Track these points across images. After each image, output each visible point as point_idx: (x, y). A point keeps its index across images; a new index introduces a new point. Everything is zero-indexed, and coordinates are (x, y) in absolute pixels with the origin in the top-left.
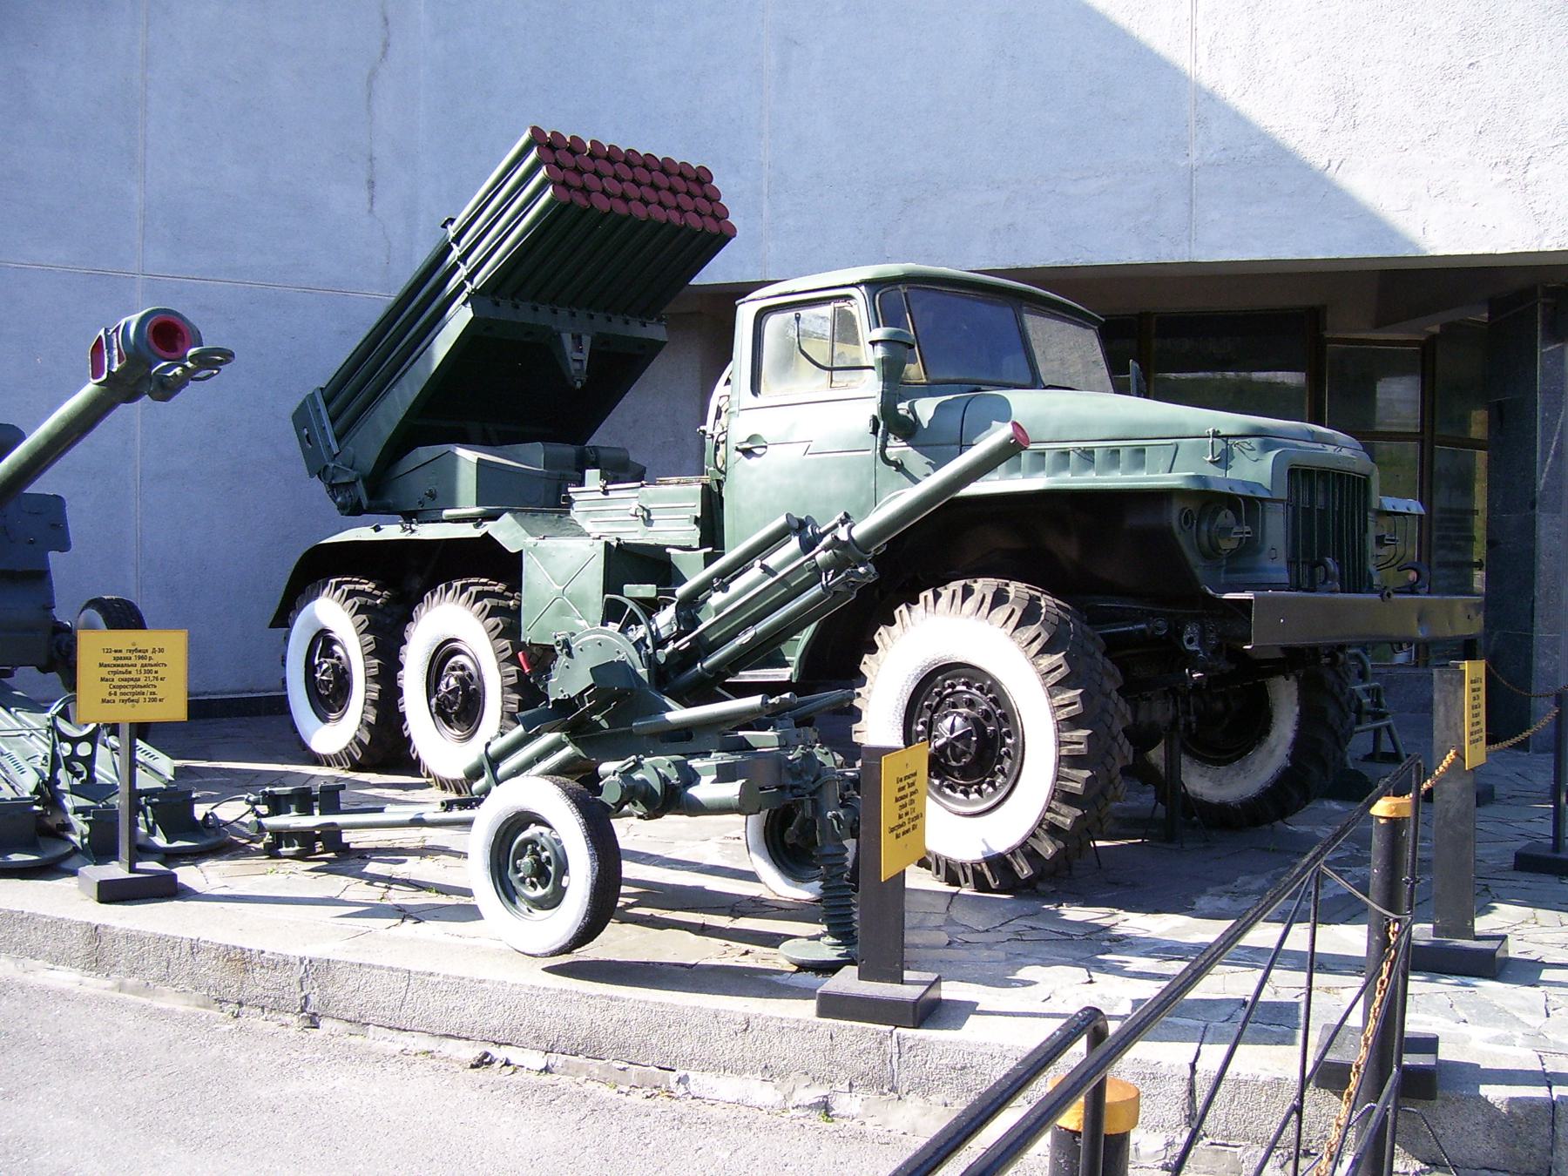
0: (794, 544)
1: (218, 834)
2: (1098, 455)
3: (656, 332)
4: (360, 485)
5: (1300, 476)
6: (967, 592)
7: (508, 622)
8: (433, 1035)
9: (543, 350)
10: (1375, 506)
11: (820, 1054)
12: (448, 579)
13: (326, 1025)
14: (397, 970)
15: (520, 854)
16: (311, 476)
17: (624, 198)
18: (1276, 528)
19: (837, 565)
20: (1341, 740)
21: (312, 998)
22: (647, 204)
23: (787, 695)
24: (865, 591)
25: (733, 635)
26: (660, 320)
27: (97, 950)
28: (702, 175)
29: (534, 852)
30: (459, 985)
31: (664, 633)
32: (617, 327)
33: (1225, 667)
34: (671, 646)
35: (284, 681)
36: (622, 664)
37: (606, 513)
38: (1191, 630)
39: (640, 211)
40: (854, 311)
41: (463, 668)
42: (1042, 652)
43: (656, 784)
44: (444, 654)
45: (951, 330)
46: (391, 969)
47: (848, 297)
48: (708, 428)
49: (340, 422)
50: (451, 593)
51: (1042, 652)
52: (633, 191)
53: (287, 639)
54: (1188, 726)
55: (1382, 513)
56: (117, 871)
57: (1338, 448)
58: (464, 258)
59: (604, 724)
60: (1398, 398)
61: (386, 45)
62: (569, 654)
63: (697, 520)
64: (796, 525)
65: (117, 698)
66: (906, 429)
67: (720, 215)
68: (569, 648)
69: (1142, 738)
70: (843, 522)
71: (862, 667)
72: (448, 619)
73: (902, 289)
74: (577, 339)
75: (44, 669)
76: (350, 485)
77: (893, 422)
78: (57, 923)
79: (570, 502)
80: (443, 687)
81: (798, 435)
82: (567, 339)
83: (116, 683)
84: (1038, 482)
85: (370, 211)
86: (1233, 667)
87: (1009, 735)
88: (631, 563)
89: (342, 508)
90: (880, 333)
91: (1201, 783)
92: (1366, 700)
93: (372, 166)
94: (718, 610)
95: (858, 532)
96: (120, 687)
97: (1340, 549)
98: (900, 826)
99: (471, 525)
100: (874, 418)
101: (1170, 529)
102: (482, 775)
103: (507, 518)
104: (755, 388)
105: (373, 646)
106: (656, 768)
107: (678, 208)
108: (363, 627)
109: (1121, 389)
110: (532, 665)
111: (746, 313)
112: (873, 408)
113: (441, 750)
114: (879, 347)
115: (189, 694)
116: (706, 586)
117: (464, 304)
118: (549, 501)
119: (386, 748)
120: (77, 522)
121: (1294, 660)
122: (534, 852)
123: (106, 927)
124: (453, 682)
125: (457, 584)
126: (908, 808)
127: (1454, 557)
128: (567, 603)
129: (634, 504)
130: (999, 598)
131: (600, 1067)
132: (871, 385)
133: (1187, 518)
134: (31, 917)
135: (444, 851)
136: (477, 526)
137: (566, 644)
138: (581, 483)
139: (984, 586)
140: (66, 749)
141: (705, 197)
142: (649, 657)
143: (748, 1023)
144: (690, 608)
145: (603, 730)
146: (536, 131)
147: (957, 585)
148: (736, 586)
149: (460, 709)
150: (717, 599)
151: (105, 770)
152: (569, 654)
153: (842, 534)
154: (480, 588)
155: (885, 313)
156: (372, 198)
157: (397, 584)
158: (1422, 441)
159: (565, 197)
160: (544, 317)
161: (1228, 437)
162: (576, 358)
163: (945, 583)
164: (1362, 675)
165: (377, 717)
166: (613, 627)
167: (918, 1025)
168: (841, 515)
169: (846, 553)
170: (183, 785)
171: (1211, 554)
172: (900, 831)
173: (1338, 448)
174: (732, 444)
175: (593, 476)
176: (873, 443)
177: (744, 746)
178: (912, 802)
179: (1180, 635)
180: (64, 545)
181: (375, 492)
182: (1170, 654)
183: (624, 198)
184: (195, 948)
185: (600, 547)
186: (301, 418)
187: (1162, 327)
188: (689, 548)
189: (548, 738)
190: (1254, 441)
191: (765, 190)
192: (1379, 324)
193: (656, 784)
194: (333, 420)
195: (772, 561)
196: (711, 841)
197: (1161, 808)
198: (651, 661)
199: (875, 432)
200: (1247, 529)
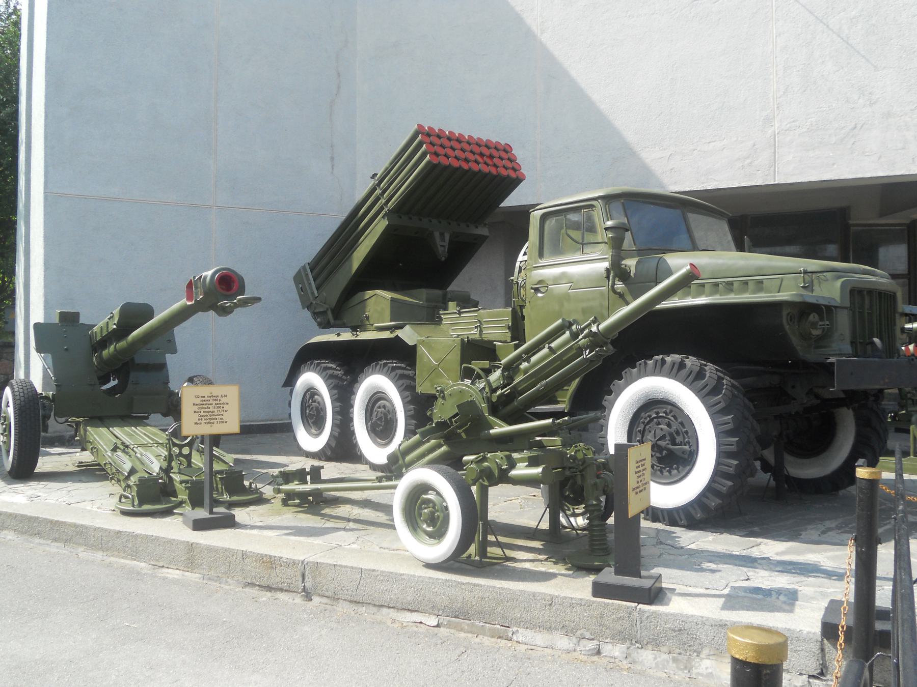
1: (256, 493)
4: (329, 313)
5: (857, 293)
7: (407, 386)
8: (375, 605)
10: (900, 310)
11: (595, 620)
13: (316, 600)
14: (356, 568)
18: (843, 322)
19: (591, 347)
21: (306, 583)
24: (608, 360)
26: (485, 225)
27: (191, 557)
30: (390, 577)
34: (499, 392)
35: (290, 415)
36: (473, 402)
37: (458, 325)
39: (475, 168)
41: (384, 407)
46: (352, 568)
47: (592, 206)
51: (709, 394)
56: (202, 513)
59: (463, 435)
61: (339, 87)
63: (509, 328)
65: (203, 422)
66: (623, 275)
71: (604, 403)
72: (377, 381)
74: (442, 234)
76: (324, 313)
77: (617, 271)
78: (171, 542)
79: (441, 320)
81: (568, 277)
82: (437, 235)
84: (702, 300)
88: (477, 351)
95: (601, 327)
98: (638, 488)
103: (407, 328)
106: (496, 458)
110: (421, 405)
111: (536, 215)
113: (375, 452)
115: (241, 422)
116: (519, 359)
117: (383, 217)
118: (431, 316)
119: (343, 448)
121: (852, 398)
123: (197, 544)
126: (641, 478)
131: (468, 625)
133: (791, 318)
134: (157, 539)
137: (442, 392)
138: (446, 309)
140: (176, 450)
144: (511, 369)
145: (459, 438)
148: (534, 359)
149: (381, 428)
150: (524, 365)
151: (198, 461)
152: (444, 398)
157: (350, 361)
158: (909, 279)
161: (812, 272)
162: (442, 245)
166: (468, 382)
167: (650, 603)
169: (596, 340)
170: (238, 469)
171: (805, 337)
172: (638, 490)
174: (528, 287)
175: (452, 305)
177: (540, 445)
180: (174, 351)
181: (339, 312)
184: (244, 555)
186: (298, 278)
187: (764, 218)
188: (505, 342)
192: (882, 215)
195: (553, 345)
196: (518, 504)
198: (488, 400)
199: (608, 277)
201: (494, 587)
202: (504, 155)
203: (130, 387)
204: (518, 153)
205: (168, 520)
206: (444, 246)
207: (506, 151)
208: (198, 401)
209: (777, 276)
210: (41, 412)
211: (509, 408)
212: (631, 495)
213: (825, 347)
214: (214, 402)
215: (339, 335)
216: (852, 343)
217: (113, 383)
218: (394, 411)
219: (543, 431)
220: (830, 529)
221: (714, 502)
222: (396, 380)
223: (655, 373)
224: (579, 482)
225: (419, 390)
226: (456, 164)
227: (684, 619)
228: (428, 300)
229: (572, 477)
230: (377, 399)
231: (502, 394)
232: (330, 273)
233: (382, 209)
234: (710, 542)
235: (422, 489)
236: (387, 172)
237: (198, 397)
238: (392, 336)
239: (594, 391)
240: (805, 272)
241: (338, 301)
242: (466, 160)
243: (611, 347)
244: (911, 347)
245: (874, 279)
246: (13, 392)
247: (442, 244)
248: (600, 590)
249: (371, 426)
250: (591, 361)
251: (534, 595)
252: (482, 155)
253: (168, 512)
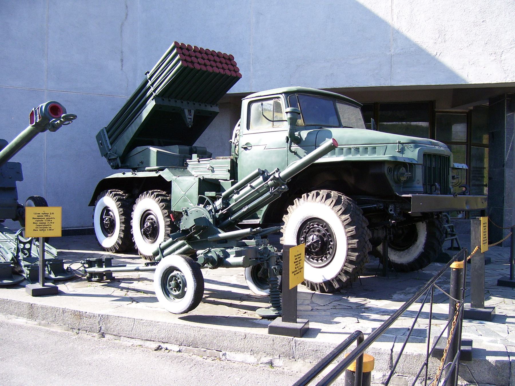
0: (261, 179)
1: (71, 274)
2: (361, 149)
3: (215, 109)
4: (118, 159)
5: (427, 156)
6: (318, 194)
7: (167, 204)
8: (142, 340)
9: (178, 115)
10: (452, 166)
11: (269, 346)
12: (147, 190)
13: (107, 336)
14: (130, 318)
15: (171, 280)
16: (102, 156)
17: (205, 65)
18: (419, 173)
19: (275, 185)
20: (440, 243)
21: (102, 328)
22: (212, 67)
23: (258, 228)
24: (284, 194)
25: (241, 208)
26: (217, 105)
27: (32, 312)
28: (231, 57)
29: (175, 280)
30: (151, 323)
31: (218, 208)
32: (203, 107)
33: (402, 219)
34: (220, 212)
35: (93, 224)
36: (204, 218)
37: (199, 168)
38: (391, 207)
39: (210, 69)
40: (280, 102)
41: (152, 219)
42: (342, 214)
43: (216, 257)
44: (146, 215)
45: (312, 108)
46: (128, 318)
47: (278, 98)
48: (233, 140)
49: (112, 139)
50: (148, 195)
51: (342, 214)
52: (208, 63)
53: (94, 210)
54: (390, 238)
55: (454, 168)
56: (38, 286)
57: (439, 147)
58: (152, 85)
59: (198, 238)
60: (459, 131)
61: (127, 15)
62: (187, 215)
63: (229, 171)
64: (262, 172)
65: (38, 229)
66: (298, 141)
67: (236, 70)
68: (187, 213)
69: (375, 242)
70: (277, 171)
71: (283, 219)
72: (147, 203)
73: (296, 95)
74: (190, 111)
75: (14, 220)
76: (115, 159)
77: (293, 138)
78: (19, 303)
79: (187, 165)
80: (145, 225)
81: (262, 143)
82: (186, 111)
83: (38, 224)
84: (341, 158)
85: (122, 69)
86: (405, 219)
87: (331, 241)
88: (207, 185)
89: (112, 167)
90: (289, 109)
91: (394, 257)
92: (449, 230)
93: (122, 54)
94: (236, 200)
95: (282, 175)
96: (39, 225)
97: (440, 180)
98: (296, 271)
99: (155, 172)
100: (287, 137)
101: (384, 174)
102: (158, 254)
103: (166, 170)
104: (248, 127)
105: (123, 212)
106: (215, 252)
107: (223, 68)
108: (119, 206)
109: (368, 128)
110: (175, 218)
111: (245, 103)
112: (287, 134)
114: (289, 114)
115: (62, 228)
116: (232, 192)
117: (152, 100)
118: (180, 165)
119: (127, 246)
120: (25, 171)
121: (425, 217)
122: (175, 280)
123: (35, 304)
124: (149, 224)
125: (150, 192)
126: (298, 265)
127: (477, 183)
128: (186, 198)
129: (208, 166)
130: (328, 196)
131: (197, 350)
132: (286, 126)
133: (390, 170)
134: (10, 301)
135: (146, 279)
136: (157, 173)
137: (186, 211)
138: (191, 159)
139: (323, 192)
140: (22, 246)
141: (232, 65)
142: (213, 216)
143: (246, 336)
144: (227, 200)
145: (198, 240)
146: (176, 43)
147: (314, 192)
148: (242, 192)
149: (151, 233)
150: (235, 196)
151: (35, 253)
152: (187, 215)
153: (277, 175)
154: (158, 193)
155: (291, 103)
156: (122, 65)
157: (130, 192)
158: (467, 145)
159: (186, 65)
160: (179, 104)
161: (403, 143)
162: (189, 117)
163: (310, 191)
164: (447, 222)
165: (124, 235)
166: (201, 206)
167: (302, 336)
168: (276, 169)
169: (278, 182)
170: (60, 258)
171: (398, 182)
172: (296, 273)
173: (439, 147)
174: (240, 146)
175: (195, 156)
176: (287, 145)
177: (244, 245)
178: (300, 263)
179: (387, 208)
180: (21, 179)
181: (123, 161)
182: (384, 215)
183: (205, 65)
184: (64, 311)
185: (197, 179)
186: (99, 137)
187: (382, 107)
188: (226, 180)
189: (180, 242)
190: (412, 145)
191: (251, 62)
192: (453, 106)
193: (216, 257)
194: (109, 138)
195: (254, 184)
197: (381, 265)
198: (214, 217)
199: (287, 142)
200: (410, 174)
219: (248, 236)
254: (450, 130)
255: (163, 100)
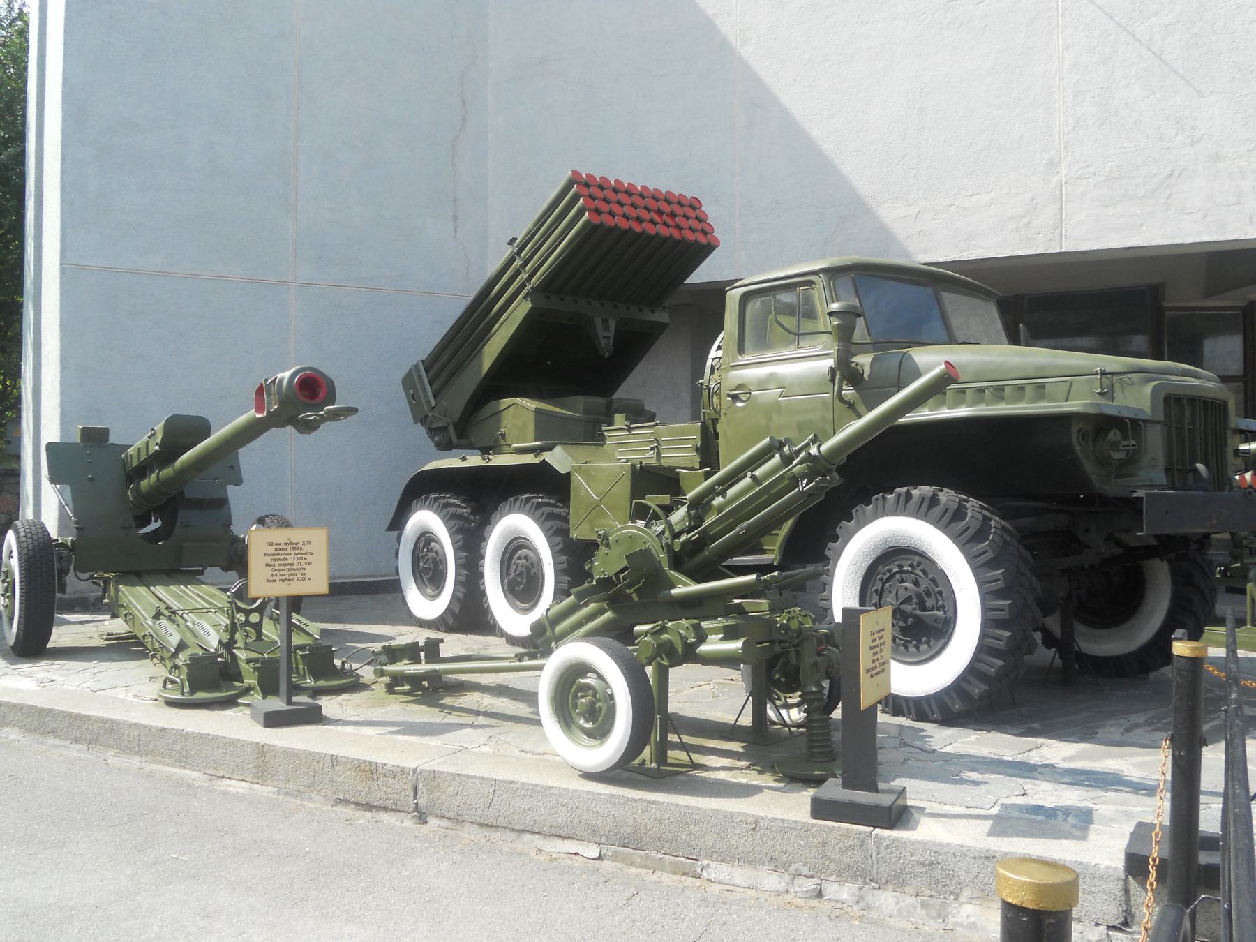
1: (351, 676)
4: (451, 429)
5: (1174, 402)
7: (558, 530)
8: (513, 830)
10: (1233, 425)
11: (814, 850)
13: (433, 822)
14: (487, 779)
18: (1155, 441)
19: (810, 476)
21: (419, 800)
24: (832, 493)
26: (665, 308)
27: (262, 764)
30: (534, 791)
34: (684, 538)
35: (397, 569)
36: (648, 551)
37: (627, 446)
39: (651, 230)
41: (526, 558)
46: (482, 778)
47: (811, 283)
51: (971, 540)
56: (276, 704)
59: (635, 597)
61: (464, 120)
63: (697, 449)
65: (278, 578)
66: (854, 377)
71: (827, 552)
72: (516, 523)
74: (605, 321)
76: (444, 429)
77: (845, 372)
78: (234, 743)
79: (604, 438)
81: (778, 380)
82: (598, 322)
84: (962, 412)
88: (653, 481)
95: (824, 448)
98: (873, 669)
103: (558, 449)
106: (680, 628)
110: (576, 556)
111: (733, 295)
115: (330, 578)
116: (711, 492)
117: (525, 297)
118: (591, 434)
119: (470, 615)
121: (1167, 546)
123: (270, 746)
126: (878, 656)
131: (641, 857)
133: (1083, 436)
134: (215, 738)
137: (605, 537)
138: (611, 423)
140: (241, 617)
144: (700, 506)
145: (628, 601)
148: (731, 492)
149: (523, 587)
150: (718, 500)
151: (271, 632)
152: (608, 545)
157: (480, 495)
158: (1246, 383)
161: (1113, 374)
162: (605, 336)
166: (641, 523)
167: (891, 826)
169: (816, 466)
170: (326, 643)
171: (1103, 462)
172: (874, 672)
174: (724, 393)
175: (619, 418)
177: (740, 611)
180: (238, 481)
181: (465, 427)
184: (334, 761)
186: (409, 382)
187: (1047, 299)
188: (692, 469)
192: (1208, 295)
195: (757, 473)
198: (669, 549)
199: (833, 380)
201: (677, 805)
202: (690, 212)
203: (178, 530)
204: (710, 209)
205: (230, 712)
206: (608, 338)
207: (693, 207)
208: (271, 550)
209: (1065, 379)
210: (56, 565)
211: (697, 559)
212: (864, 678)
213: (1130, 476)
214: (293, 552)
215: (464, 459)
216: (1167, 470)
217: (155, 525)
218: (539, 564)
220: (1136, 726)
221: (978, 689)
222: (543, 521)
223: (897, 511)
224: (793, 661)
225: (574, 535)
226: (624, 225)
227: (937, 848)
228: (586, 412)
229: (783, 653)
230: (516, 547)
231: (688, 541)
232: (452, 375)
233: (523, 286)
234: (973, 743)
235: (578, 670)
236: (531, 236)
237: (271, 544)
238: (537, 460)
239: (814, 537)
240: (1103, 373)
241: (464, 413)
242: (639, 220)
243: (837, 476)
244: (1248, 476)
245: (1197, 382)
246: (18, 538)
247: (606, 334)
248: (821, 809)
249: (508, 584)
250: (810, 495)
251: (732, 815)
252: (660, 212)
253: (230, 703)
254: (1201, 345)
255: (562, 299)
